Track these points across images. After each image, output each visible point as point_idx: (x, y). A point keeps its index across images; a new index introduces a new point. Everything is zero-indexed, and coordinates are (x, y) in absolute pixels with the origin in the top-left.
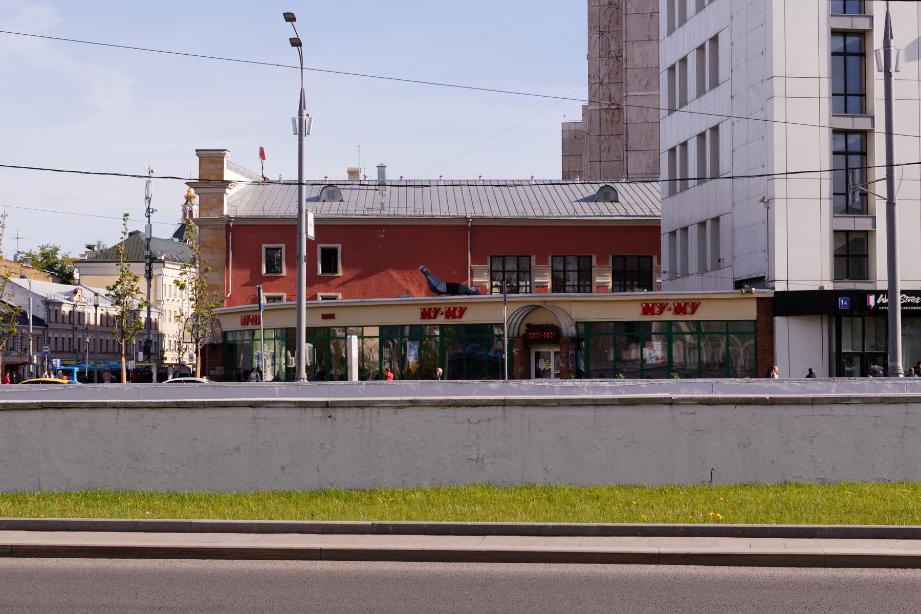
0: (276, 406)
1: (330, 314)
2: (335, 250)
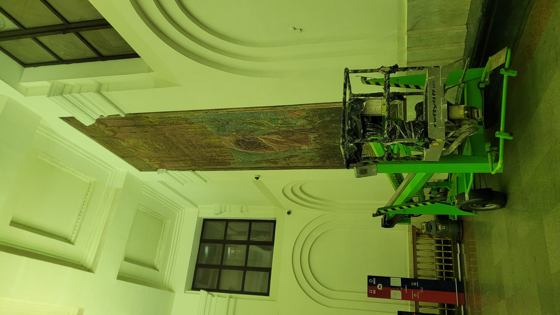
0: (262, 109)
2: (177, 213)
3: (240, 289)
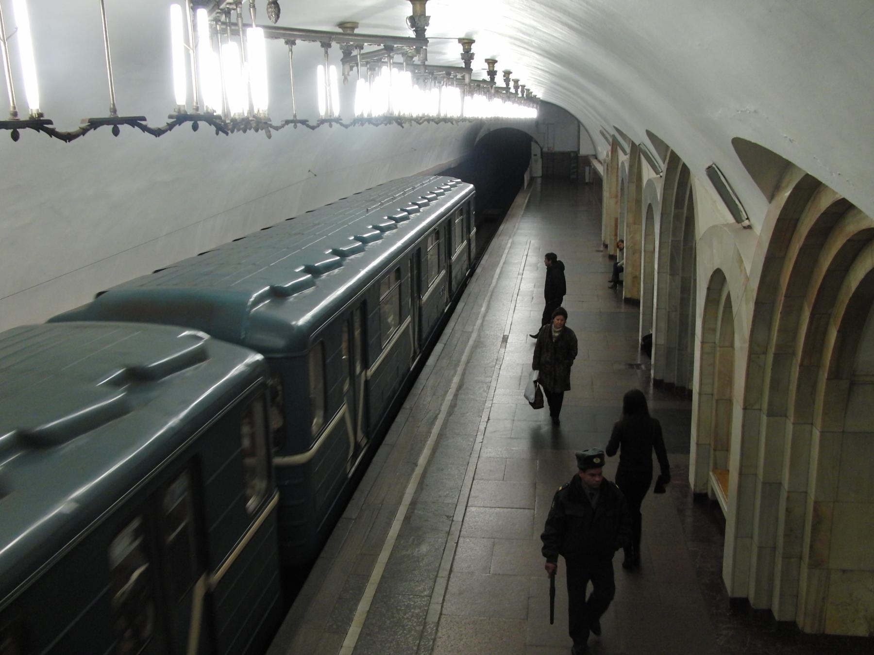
1: (471, 62)
3: (658, 344)
